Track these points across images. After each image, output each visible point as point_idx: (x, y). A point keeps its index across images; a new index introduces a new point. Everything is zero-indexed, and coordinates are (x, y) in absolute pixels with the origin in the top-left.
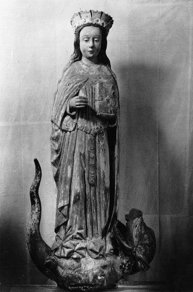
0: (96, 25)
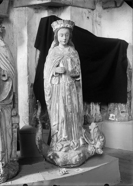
0: (67, 28)
